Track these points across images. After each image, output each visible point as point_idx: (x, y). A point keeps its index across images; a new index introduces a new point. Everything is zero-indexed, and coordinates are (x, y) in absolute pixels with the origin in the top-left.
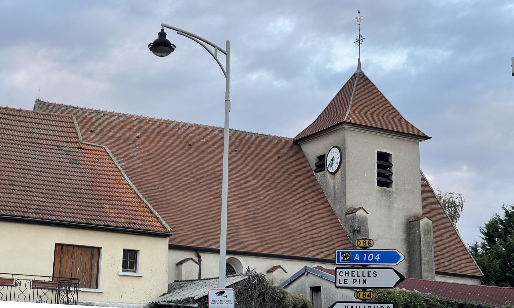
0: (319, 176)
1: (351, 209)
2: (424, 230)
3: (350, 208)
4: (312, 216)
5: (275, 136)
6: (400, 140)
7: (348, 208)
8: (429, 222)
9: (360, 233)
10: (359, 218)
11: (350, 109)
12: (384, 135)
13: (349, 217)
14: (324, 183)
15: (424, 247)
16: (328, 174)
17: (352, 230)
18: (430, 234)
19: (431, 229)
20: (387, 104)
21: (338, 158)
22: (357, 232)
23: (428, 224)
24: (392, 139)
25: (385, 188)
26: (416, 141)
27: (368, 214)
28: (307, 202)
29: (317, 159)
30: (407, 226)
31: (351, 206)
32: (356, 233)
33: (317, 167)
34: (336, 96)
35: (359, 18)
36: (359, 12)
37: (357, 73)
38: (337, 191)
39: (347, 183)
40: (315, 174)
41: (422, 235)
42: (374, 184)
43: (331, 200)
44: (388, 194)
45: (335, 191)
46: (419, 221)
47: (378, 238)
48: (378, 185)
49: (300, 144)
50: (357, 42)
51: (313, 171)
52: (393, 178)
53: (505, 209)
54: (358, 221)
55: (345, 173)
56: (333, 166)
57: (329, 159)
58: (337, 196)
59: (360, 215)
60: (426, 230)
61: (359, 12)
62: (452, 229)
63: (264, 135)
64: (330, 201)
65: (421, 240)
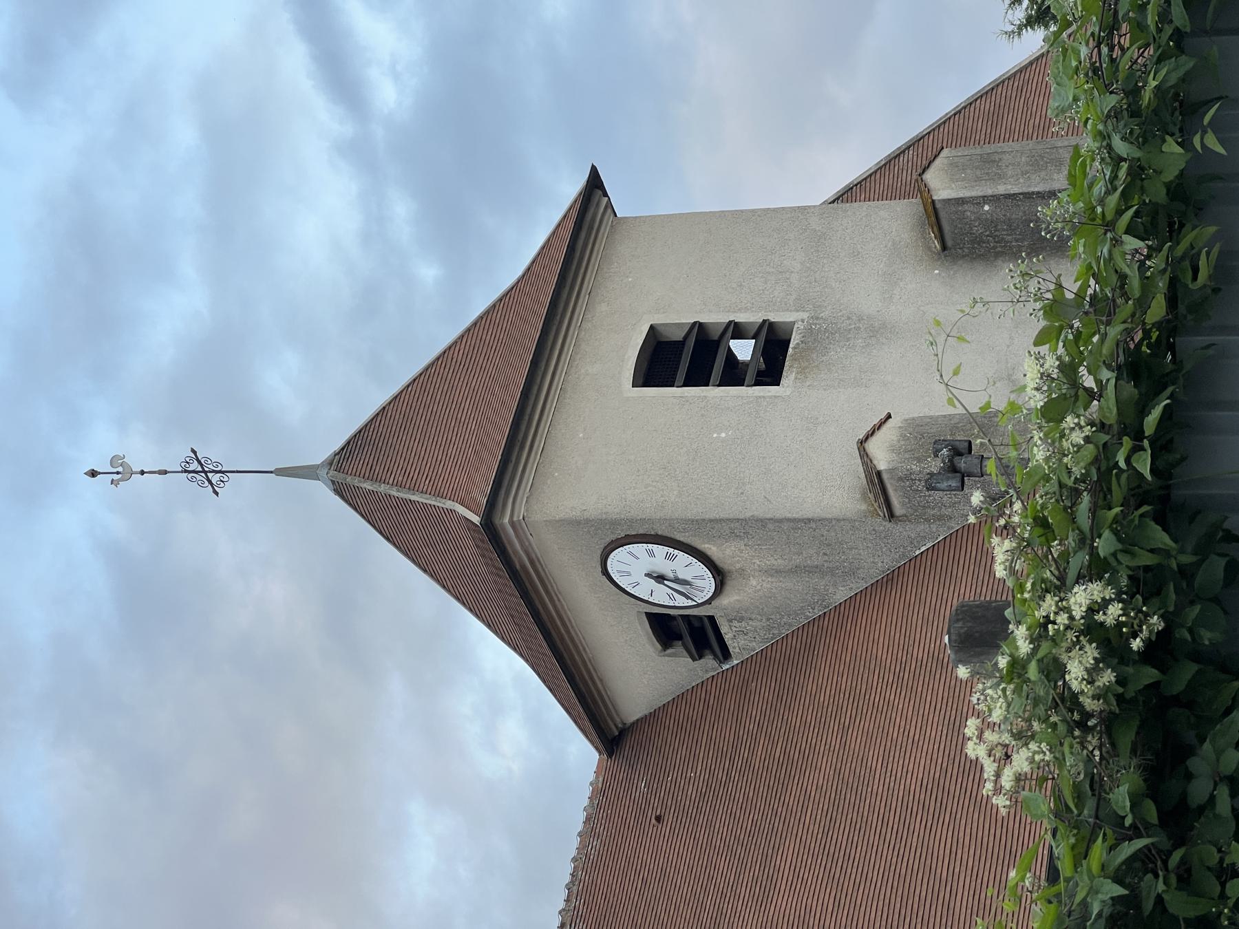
0: (742, 641)
1: (871, 496)
2: (978, 179)
3: (864, 497)
4: (897, 670)
5: (580, 835)
6: (592, 294)
7: (864, 507)
8: (946, 161)
9: (966, 444)
10: (907, 456)
11: (449, 504)
12: (566, 358)
13: (903, 504)
14: (768, 620)
15: (1055, 176)
16: (726, 600)
17: (948, 479)
18: (997, 157)
19: (978, 151)
20: (456, 355)
21: (651, 554)
22: (957, 459)
23: (953, 166)
24: (586, 325)
25: (790, 350)
26: (605, 230)
27: (889, 416)
28: (842, 695)
29: (669, 651)
30: (964, 256)
31: (858, 496)
32: (962, 463)
33: (707, 652)
34: (425, 571)
35: (118, 473)
36: (93, 474)
37: (333, 482)
38: (798, 560)
39: (756, 513)
40: (736, 662)
41: (1001, 189)
42: (770, 397)
43: (835, 585)
44: (819, 336)
45: (796, 570)
46: (938, 206)
47: (1009, 376)
48: (777, 383)
49: (617, 727)
50: (214, 482)
51: (725, 667)
52: (752, 320)
53: (1020, 28)
54: (919, 460)
55: (711, 521)
56: (689, 578)
57: (662, 596)
58: (818, 560)
59: (892, 449)
60: (978, 172)
61: (93, 474)
62: (999, 92)
63: (572, 882)
64: (841, 594)
65: (1021, 191)
